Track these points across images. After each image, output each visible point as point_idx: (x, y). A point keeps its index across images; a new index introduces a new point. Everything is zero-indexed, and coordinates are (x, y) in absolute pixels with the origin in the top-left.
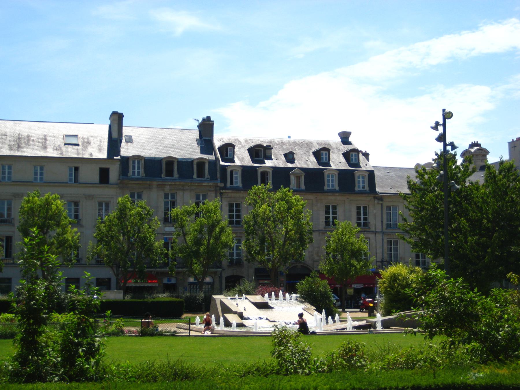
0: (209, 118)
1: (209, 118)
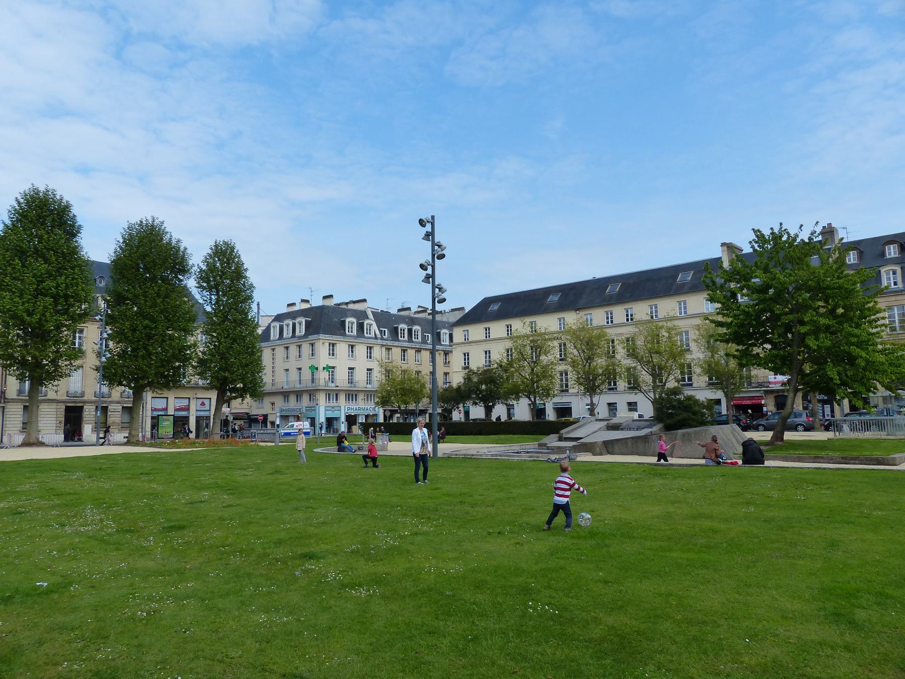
0: (830, 224)
1: (830, 224)
